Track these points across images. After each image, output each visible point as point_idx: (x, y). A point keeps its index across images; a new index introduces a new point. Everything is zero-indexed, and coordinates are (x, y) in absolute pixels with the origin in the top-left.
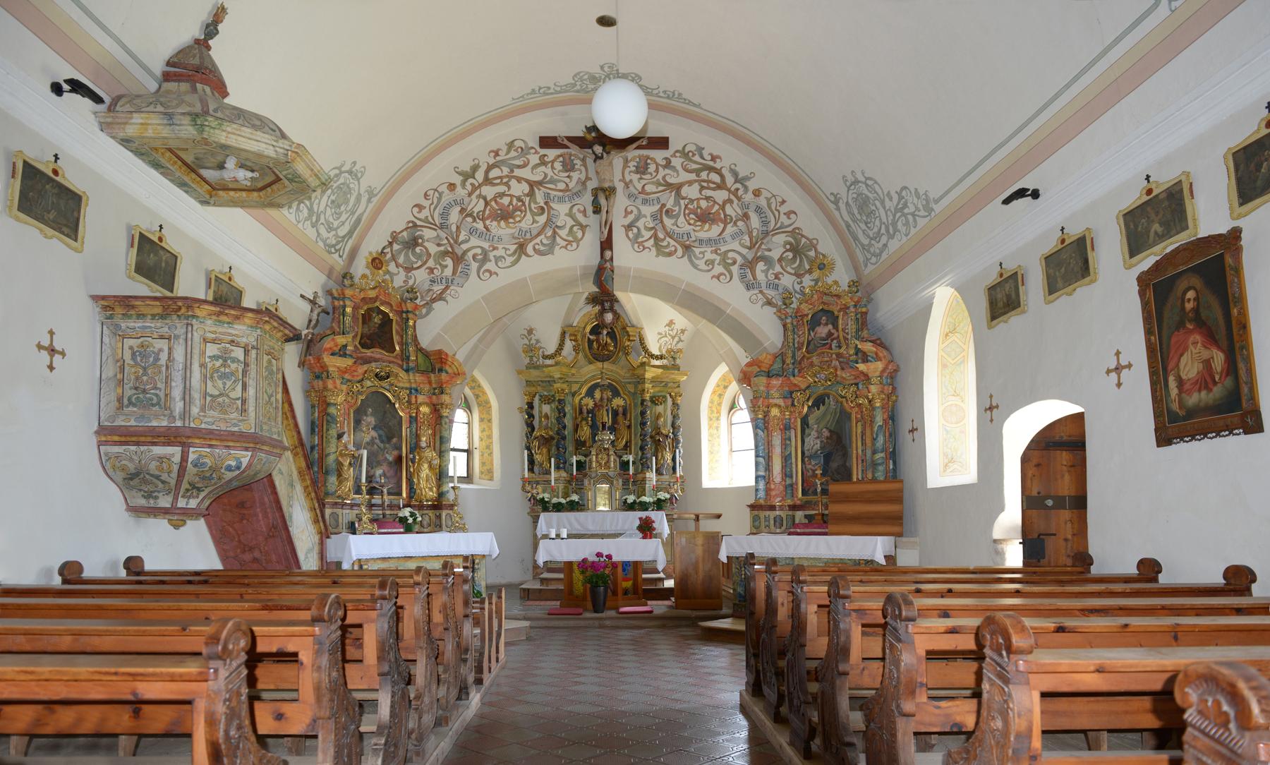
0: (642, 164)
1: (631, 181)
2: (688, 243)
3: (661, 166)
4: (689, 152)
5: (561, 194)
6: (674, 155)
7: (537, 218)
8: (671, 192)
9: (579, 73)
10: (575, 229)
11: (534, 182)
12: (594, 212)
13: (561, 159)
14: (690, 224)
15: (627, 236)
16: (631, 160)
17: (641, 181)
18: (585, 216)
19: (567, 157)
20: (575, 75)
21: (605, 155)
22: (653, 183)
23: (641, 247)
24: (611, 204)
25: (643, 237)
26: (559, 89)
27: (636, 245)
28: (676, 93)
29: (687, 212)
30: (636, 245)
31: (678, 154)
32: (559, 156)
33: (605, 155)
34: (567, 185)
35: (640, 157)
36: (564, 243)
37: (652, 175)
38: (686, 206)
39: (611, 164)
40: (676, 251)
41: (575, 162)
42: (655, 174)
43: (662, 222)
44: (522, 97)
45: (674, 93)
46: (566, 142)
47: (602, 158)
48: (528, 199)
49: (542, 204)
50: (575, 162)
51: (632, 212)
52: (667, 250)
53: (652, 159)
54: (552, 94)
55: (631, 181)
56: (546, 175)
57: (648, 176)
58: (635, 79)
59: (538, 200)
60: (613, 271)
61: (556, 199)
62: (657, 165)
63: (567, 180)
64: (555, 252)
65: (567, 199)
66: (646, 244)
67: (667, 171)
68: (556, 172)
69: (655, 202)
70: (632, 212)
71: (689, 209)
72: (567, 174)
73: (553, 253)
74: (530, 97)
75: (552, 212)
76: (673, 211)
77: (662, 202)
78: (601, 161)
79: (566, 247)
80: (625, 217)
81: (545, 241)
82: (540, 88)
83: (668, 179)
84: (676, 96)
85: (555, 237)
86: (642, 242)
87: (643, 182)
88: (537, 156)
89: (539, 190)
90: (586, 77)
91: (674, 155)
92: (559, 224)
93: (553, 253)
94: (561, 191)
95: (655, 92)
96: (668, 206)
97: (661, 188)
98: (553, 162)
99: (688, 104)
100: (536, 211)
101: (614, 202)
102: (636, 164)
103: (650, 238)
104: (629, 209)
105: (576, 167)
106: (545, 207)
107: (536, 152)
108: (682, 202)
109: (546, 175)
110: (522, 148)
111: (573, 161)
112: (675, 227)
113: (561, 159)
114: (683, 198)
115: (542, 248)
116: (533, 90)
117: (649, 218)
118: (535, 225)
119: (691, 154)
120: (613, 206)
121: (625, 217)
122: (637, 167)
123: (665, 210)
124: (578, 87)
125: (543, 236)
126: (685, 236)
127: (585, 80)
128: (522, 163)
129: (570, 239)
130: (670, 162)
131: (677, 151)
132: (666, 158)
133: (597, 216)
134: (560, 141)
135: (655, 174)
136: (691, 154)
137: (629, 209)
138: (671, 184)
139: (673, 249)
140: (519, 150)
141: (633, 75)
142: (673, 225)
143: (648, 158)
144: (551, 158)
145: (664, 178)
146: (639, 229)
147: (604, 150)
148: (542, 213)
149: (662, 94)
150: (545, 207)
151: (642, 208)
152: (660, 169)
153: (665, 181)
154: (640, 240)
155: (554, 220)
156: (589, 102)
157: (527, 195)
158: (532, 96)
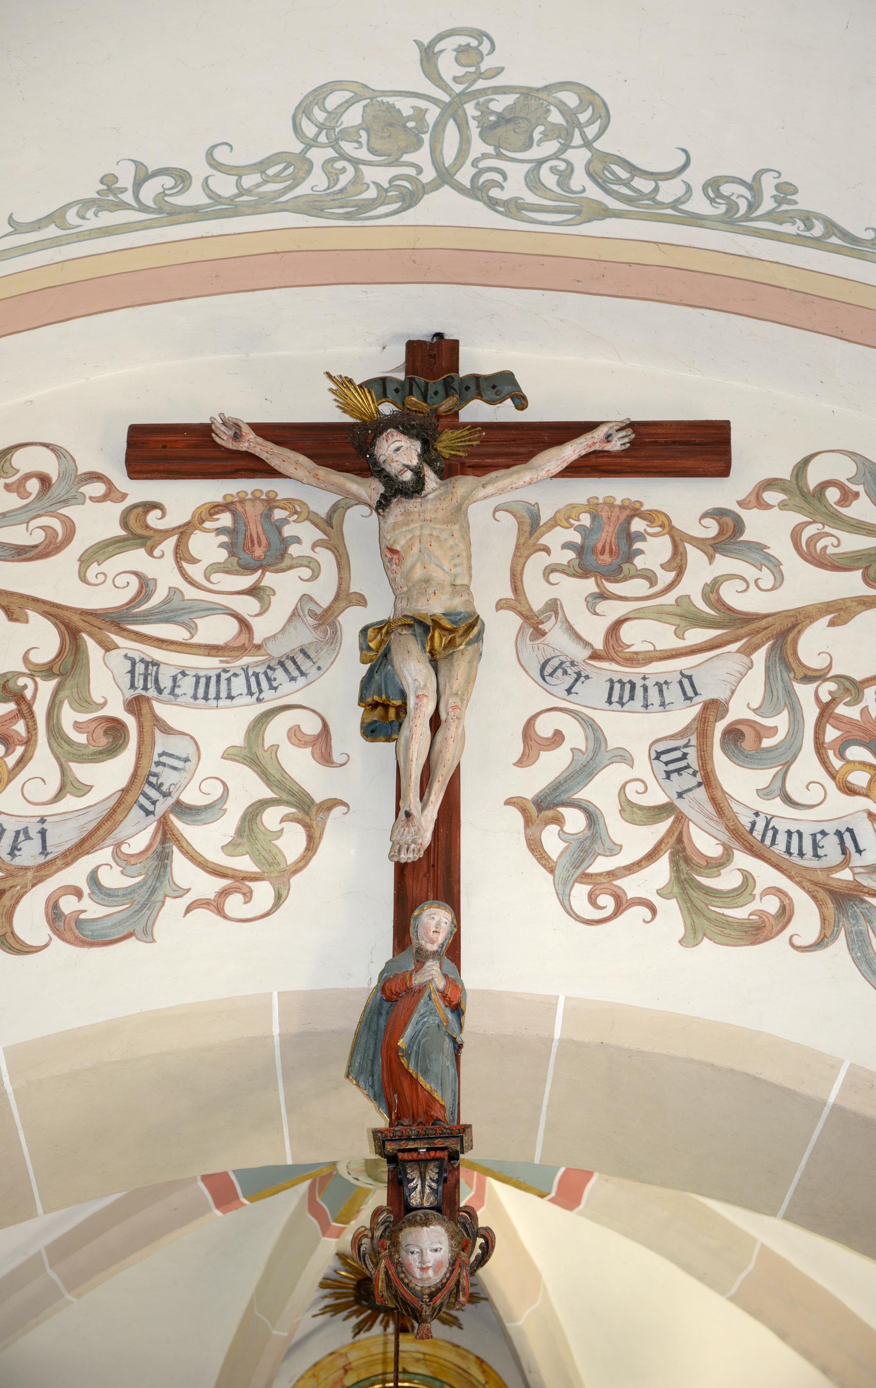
0: (607, 534)
1: (554, 607)
2: (845, 875)
3: (698, 543)
4: (824, 485)
5: (210, 664)
6: (756, 500)
7: (82, 771)
8: (748, 651)
9: (319, 95)
10: (271, 818)
11: (85, 613)
12: (371, 732)
13: (225, 520)
14: (849, 790)
15: (535, 847)
16: (554, 523)
17: (603, 606)
18: (326, 758)
19: (253, 511)
20: (304, 109)
21: (431, 479)
22: (660, 615)
23: (607, 901)
24: (457, 683)
25: (615, 849)
26: (226, 186)
27: (581, 891)
28: (768, 184)
29: (831, 734)
30: (581, 891)
31: (772, 497)
32: (215, 509)
33: (431, 479)
34: (244, 624)
35: (593, 508)
36: (211, 886)
37: (653, 582)
38: (826, 711)
39: (459, 513)
40: (786, 913)
41: (287, 531)
42: (669, 576)
43: (708, 781)
44: (56, 217)
45: (754, 187)
46: (252, 443)
47: (416, 488)
48: (47, 687)
49: (116, 709)
50: (287, 531)
51: (558, 737)
52: (740, 913)
53: (650, 517)
54: (196, 213)
55: (554, 607)
56: (146, 586)
57: (636, 587)
58: (580, 513)
59: (96, 696)
60: (457, 1010)
61: (187, 685)
62: (678, 540)
63: (247, 606)
64: (158, 930)
65: (238, 686)
66: (631, 886)
67: (724, 564)
68: (195, 571)
69: (673, 693)
70: (558, 737)
71: (841, 721)
72: (247, 581)
73: (147, 935)
74: (94, 221)
75: (162, 743)
76: (760, 732)
77: (707, 693)
78: (413, 505)
79: (216, 906)
80: (524, 761)
81: (112, 878)
82: (143, 176)
83: (730, 595)
84: (768, 204)
85: (163, 859)
86: (612, 874)
87: (612, 611)
88: (116, 509)
89: (108, 647)
90: (353, 117)
91: (756, 500)
92: (191, 797)
93: (147, 935)
94: (212, 650)
95: (669, 191)
96: (737, 711)
97: (697, 636)
98: (184, 532)
99: (817, 243)
100: (81, 738)
101: (470, 680)
102: (576, 538)
103: (652, 856)
104: (544, 728)
105: (294, 550)
106: (130, 721)
107: (111, 494)
108: (804, 692)
109: (146, 586)
110: (45, 481)
111: (278, 527)
112: (776, 807)
113: (225, 520)
114: (811, 677)
115: (92, 909)
116: (109, 181)
117: (643, 767)
118: (70, 803)
119: (833, 495)
120: (464, 696)
121: (524, 761)
122: (580, 550)
123: (720, 727)
124: (317, 181)
125: (104, 855)
126: (830, 846)
127: (349, 134)
128: (38, 537)
129: (244, 863)
130: (739, 526)
131: (770, 484)
132: (718, 514)
133: (384, 749)
134: (224, 439)
135: (669, 576)
136: (833, 495)
137: (544, 728)
138: (744, 620)
139: (772, 905)
140: (33, 486)
141: (571, 99)
142: (765, 793)
143: (634, 511)
144: (177, 516)
145: (712, 591)
146: (592, 817)
147: (428, 455)
148: (113, 750)
149: (699, 204)
150: (130, 721)
151: (606, 720)
152: (694, 555)
153: (719, 604)
154: (601, 865)
155: (168, 778)
156: (436, 898)
157: (48, 671)
158: (108, 219)
